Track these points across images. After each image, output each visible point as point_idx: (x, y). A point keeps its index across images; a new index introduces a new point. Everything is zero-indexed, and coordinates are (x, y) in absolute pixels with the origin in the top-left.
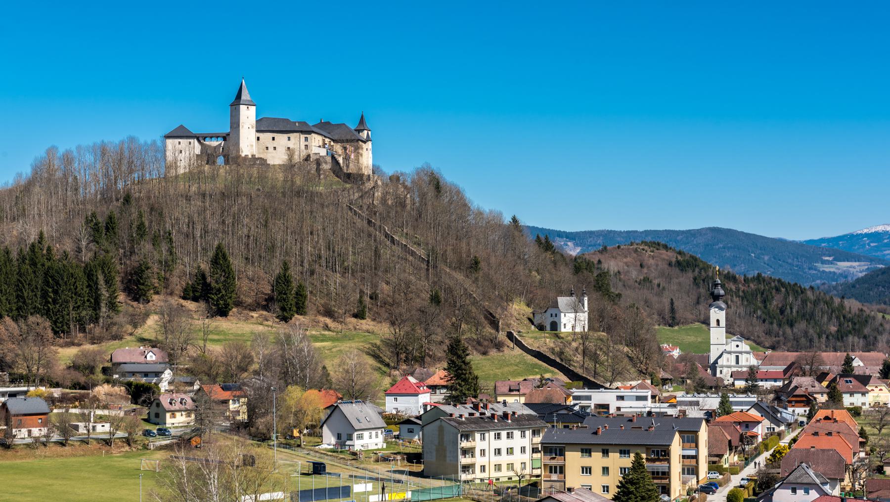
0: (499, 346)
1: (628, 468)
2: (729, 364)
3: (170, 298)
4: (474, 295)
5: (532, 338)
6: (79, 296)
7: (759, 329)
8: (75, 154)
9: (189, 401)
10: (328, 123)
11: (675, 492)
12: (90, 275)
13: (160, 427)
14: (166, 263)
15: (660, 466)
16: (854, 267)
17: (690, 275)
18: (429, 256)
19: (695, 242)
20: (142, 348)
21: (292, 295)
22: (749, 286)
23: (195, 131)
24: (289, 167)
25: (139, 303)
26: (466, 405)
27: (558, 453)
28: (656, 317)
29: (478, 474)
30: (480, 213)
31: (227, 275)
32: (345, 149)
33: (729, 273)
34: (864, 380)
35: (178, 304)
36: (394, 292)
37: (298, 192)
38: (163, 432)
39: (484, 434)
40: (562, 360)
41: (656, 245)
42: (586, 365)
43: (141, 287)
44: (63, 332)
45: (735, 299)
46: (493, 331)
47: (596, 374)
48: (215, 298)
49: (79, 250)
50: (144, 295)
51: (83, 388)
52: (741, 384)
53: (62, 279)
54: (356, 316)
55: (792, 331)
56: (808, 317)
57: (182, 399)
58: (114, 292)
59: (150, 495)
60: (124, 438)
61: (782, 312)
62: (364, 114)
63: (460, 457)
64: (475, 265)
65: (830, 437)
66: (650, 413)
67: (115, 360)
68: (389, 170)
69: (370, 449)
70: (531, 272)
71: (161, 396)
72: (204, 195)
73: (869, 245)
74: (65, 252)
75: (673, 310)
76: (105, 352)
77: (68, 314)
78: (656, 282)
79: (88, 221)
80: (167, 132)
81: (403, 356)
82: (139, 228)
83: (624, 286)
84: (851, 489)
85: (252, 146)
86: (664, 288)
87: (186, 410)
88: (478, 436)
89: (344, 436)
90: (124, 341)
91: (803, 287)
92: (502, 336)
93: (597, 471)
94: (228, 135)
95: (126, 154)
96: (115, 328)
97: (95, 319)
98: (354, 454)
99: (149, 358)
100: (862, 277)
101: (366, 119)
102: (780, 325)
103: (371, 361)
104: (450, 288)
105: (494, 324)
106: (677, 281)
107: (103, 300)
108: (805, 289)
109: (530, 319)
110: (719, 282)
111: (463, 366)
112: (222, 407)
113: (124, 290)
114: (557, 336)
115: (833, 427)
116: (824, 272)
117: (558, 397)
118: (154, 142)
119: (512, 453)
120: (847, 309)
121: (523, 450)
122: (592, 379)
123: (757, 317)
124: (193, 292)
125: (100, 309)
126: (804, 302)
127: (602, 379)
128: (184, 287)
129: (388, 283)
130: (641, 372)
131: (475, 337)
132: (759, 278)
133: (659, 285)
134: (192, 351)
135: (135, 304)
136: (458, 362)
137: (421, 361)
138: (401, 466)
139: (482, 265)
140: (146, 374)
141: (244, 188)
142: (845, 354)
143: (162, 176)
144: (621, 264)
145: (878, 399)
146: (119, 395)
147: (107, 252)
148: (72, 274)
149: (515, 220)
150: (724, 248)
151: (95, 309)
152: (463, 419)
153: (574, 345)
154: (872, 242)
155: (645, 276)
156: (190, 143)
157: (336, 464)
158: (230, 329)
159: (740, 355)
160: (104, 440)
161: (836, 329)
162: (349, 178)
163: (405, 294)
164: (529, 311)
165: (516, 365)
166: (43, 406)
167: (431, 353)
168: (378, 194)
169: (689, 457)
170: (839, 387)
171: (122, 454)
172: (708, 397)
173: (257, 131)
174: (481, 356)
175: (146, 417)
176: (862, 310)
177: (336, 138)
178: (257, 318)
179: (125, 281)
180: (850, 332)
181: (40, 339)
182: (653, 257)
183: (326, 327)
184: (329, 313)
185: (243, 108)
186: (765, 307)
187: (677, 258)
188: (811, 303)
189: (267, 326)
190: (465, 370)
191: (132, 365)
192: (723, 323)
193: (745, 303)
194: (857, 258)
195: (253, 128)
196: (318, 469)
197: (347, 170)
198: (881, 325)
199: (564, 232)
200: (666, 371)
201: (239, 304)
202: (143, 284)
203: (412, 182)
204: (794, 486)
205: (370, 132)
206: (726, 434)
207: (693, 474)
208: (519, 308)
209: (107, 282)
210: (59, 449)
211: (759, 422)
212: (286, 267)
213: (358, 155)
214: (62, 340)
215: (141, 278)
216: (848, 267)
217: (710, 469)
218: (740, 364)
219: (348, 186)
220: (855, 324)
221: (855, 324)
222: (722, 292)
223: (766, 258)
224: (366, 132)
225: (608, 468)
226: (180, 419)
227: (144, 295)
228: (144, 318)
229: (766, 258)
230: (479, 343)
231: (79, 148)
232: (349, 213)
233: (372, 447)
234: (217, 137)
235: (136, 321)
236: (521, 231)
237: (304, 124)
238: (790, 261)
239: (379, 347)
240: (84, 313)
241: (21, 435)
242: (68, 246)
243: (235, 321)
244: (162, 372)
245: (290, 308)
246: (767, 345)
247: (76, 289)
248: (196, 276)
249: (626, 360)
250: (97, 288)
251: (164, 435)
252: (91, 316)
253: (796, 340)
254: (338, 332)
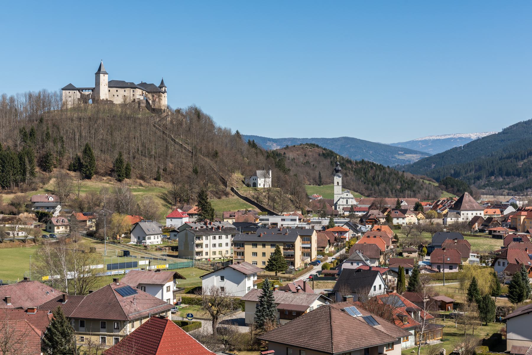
0: (227, 194)
1: (273, 253)
2: (343, 204)
3: (62, 170)
4: (215, 169)
5: (243, 190)
6: (15, 168)
7: (362, 187)
8: (15, 97)
9: (66, 220)
10: (145, 83)
11: (297, 264)
12: (21, 158)
13: (52, 233)
14: (60, 152)
16: (414, 157)
17: (329, 160)
18: (193, 150)
19: (336, 144)
20: (46, 195)
21: (123, 168)
22: (358, 166)
23: (77, 86)
24: (124, 105)
25: (46, 172)
26: (201, 223)
27: (241, 246)
28: (312, 181)
29: (204, 256)
30: (220, 129)
31: (91, 158)
32: (153, 96)
33: (348, 159)
34: (404, 212)
35: (66, 173)
36: (175, 168)
37: (128, 118)
38: (52, 236)
39: (207, 237)
40: (257, 201)
41: (313, 145)
42: (269, 204)
43: (48, 164)
44: (7, 186)
45: (351, 172)
46: (224, 187)
47: (274, 208)
48: (85, 170)
49: (16, 146)
50: (49, 168)
52: (347, 214)
53: (7, 160)
54: (155, 179)
55: (378, 188)
56: (386, 181)
57: (63, 220)
58: (33, 167)
59: (32, 266)
60: (32, 239)
61: (374, 178)
63: (195, 248)
64: (216, 154)
65: (375, 238)
66: (297, 227)
67: (32, 201)
68: (174, 107)
69: (154, 244)
70: (244, 158)
71: (52, 218)
72: (80, 119)
73: (422, 146)
74: (8, 147)
75: (320, 177)
76: (28, 197)
77: (10, 178)
78: (312, 163)
79: (21, 131)
80: (63, 87)
81: (178, 199)
82: (47, 135)
83: (297, 165)
84: (384, 263)
85: (106, 94)
86: (316, 167)
87: (64, 225)
88: (204, 238)
89: (141, 239)
90: (38, 191)
91: (384, 166)
92: (228, 189)
93: (260, 254)
94: (94, 88)
95: (42, 97)
96: (33, 185)
97: (24, 180)
98: (145, 247)
99: (50, 200)
100: (417, 162)
102: (372, 185)
103: (163, 202)
104: (202, 165)
105: (225, 184)
106: (323, 163)
107: (28, 171)
108: (385, 167)
109: (243, 181)
110: (339, 164)
111: (206, 204)
112: (83, 224)
113: (39, 166)
114: (256, 190)
115: (379, 233)
116: (399, 159)
118: (55, 92)
119: (221, 246)
120: (406, 177)
121: (227, 244)
122: (272, 211)
123: (361, 181)
124: (74, 167)
125: (26, 175)
126: (384, 174)
127: (277, 211)
128: (69, 164)
129: (172, 163)
130: (297, 207)
131: (215, 190)
132: (363, 162)
133: (313, 165)
134: (72, 196)
135: (44, 173)
136: (203, 202)
137: (188, 202)
138: (169, 253)
139: (219, 154)
140: (48, 208)
141: (101, 115)
142: (396, 199)
143: (59, 109)
144: (295, 155)
145: (410, 221)
146: (32, 218)
147: (30, 147)
148: (11, 157)
149: (237, 132)
150: (350, 147)
151: (23, 175)
152: (197, 229)
153: (264, 194)
154: (423, 145)
155: (307, 160)
156: (75, 92)
157: (136, 251)
158: (92, 186)
159: (348, 200)
160: (22, 240)
161: (400, 187)
162: (154, 111)
163: (181, 169)
164: (242, 177)
165: (235, 204)
167: (193, 198)
168: (169, 119)
169: (307, 248)
171: (31, 247)
172: (326, 219)
173: (109, 87)
174: (218, 200)
175: (45, 229)
176: (412, 178)
177: (149, 91)
178: (106, 180)
179: (39, 161)
180: (406, 189)
182: (311, 151)
185: (101, 75)
186: (366, 176)
187: (323, 152)
188: (388, 174)
189: (110, 184)
190: (206, 206)
191: (42, 203)
192: (340, 184)
193: (356, 174)
195: (106, 85)
196: (126, 254)
197: (154, 107)
198: (422, 185)
199: (272, 139)
200: (309, 207)
201: (97, 173)
202: (48, 163)
203: (186, 113)
204: (352, 261)
205: (166, 88)
206: (327, 237)
207: (309, 256)
208: (237, 176)
209: (30, 161)
211: (347, 232)
212: (120, 155)
213: (160, 100)
214: (6, 191)
215: (47, 160)
216: (411, 157)
217: (318, 254)
218: (348, 204)
219: (153, 115)
220: (409, 185)
221: (409, 185)
222: (340, 168)
223: (371, 152)
224: (164, 88)
225: (265, 253)
226: (62, 229)
227: (49, 168)
228: (48, 179)
229: (371, 152)
230: (217, 193)
232: (154, 128)
233: (155, 243)
234: (89, 90)
236: (240, 138)
237: (133, 83)
238: (382, 154)
239: (167, 195)
240: (18, 177)
242: (10, 143)
243: (95, 182)
244: (56, 207)
245: (123, 175)
246: (366, 194)
247: (13, 165)
248: (75, 159)
249: (289, 201)
250: (24, 165)
251: (53, 237)
252: (22, 178)
253: (380, 192)
254: (146, 187)
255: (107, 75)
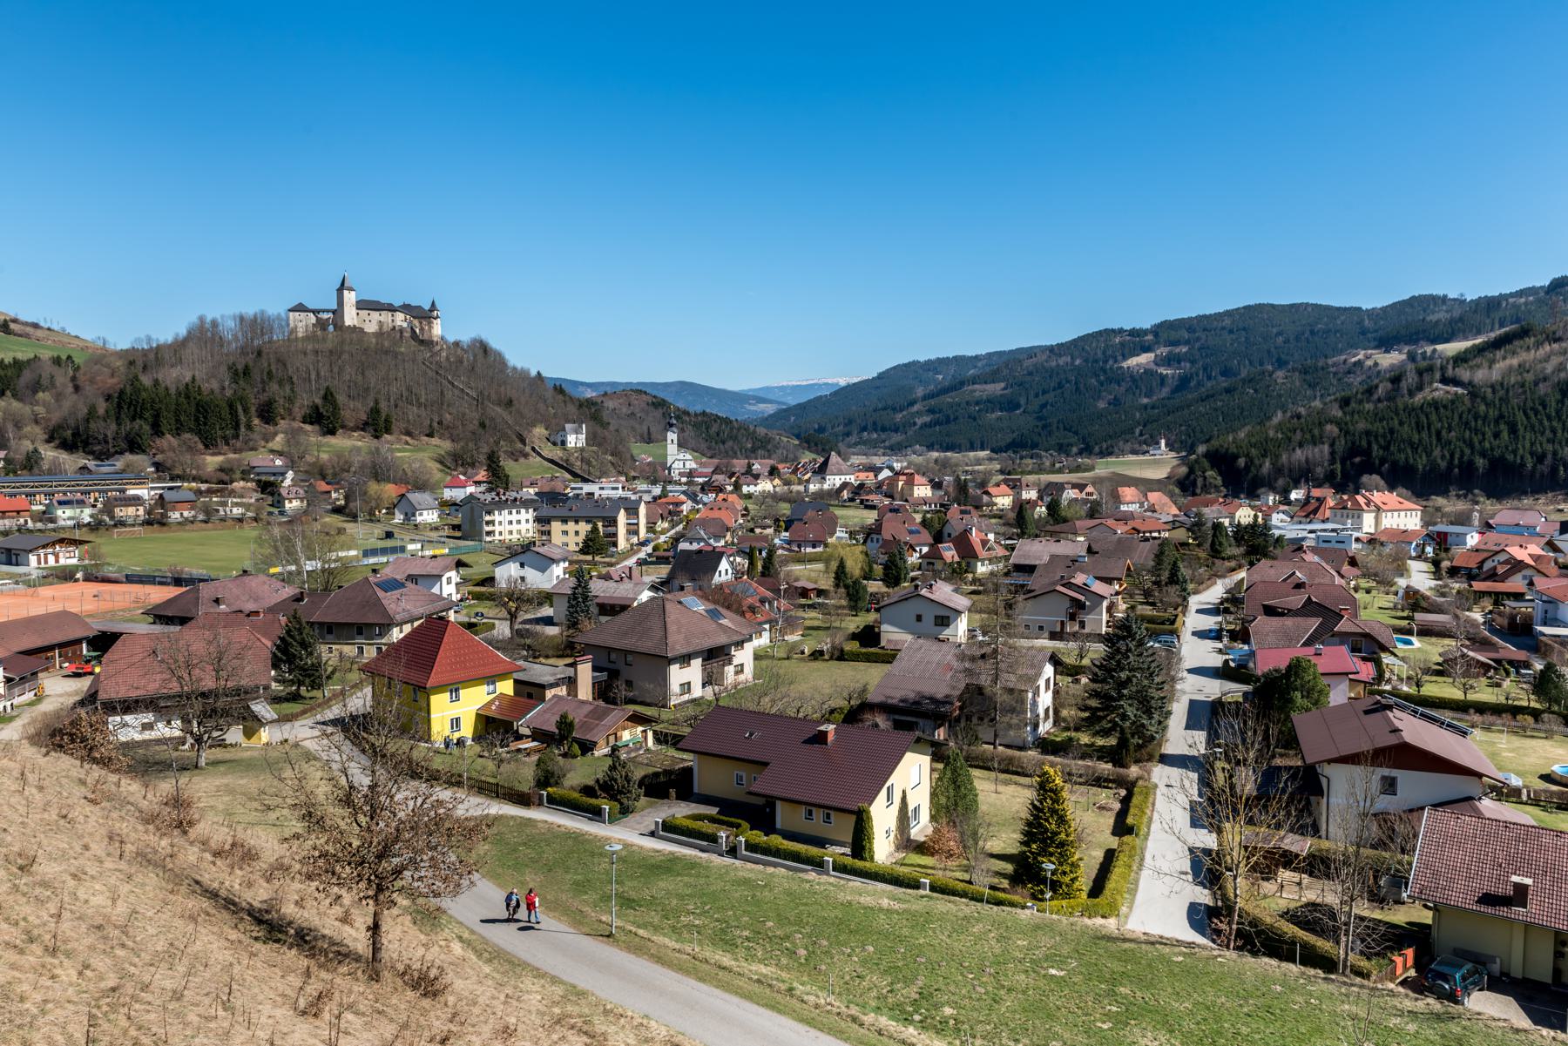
0: (526, 456)
7: (703, 446)
12: (231, 406)
15: (611, 529)
17: (661, 411)
23: (311, 307)
24: (380, 334)
29: (497, 537)
30: (515, 369)
34: (757, 477)
38: (282, 513)
41: (640, 392)
47: (589, 474)
49: (224, 388)
51: (225, 483)
54: (427, 435)
64: (510, 403)
68: (451, 339)
75: (649, 433)
79: (230, 368)
89: (410, 515)
92: (528, 449)
97: (237, 437)
101: (437, 303)
103: (439, 466)
105: (523, 441)
112: (326, 496)
117: (558, 486)
126: (732, 429)
132: (704, 413)
136: (494, 466)
137: (473, 465)
139: (515, 402)
140: (274, 474)
166: (192, 497)
168: (444, 354)
170: (741, 482)
181: (190, 449)
183: (407, 443)
184: (409, 434)
194: (770, 402)
201: (343, 427)
208: (540, 431)
209: (244, 411)
210: (204, 525)
212: (377, 402)
213: (431, 328)
231: (222, 317)
233: (430, 521)
235: (268, 438)
241: (175, 516)
242: (215, 385)
253: (727, 452)
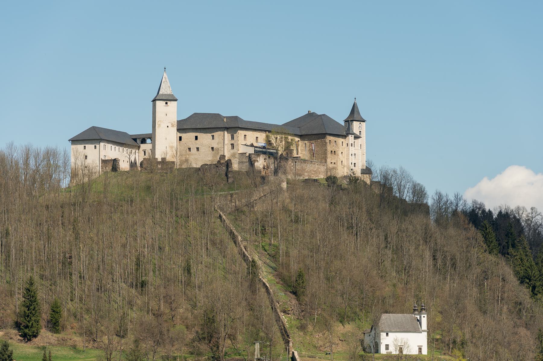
62: (357, 101)
195: (173, 126)
255: (175, 103)
